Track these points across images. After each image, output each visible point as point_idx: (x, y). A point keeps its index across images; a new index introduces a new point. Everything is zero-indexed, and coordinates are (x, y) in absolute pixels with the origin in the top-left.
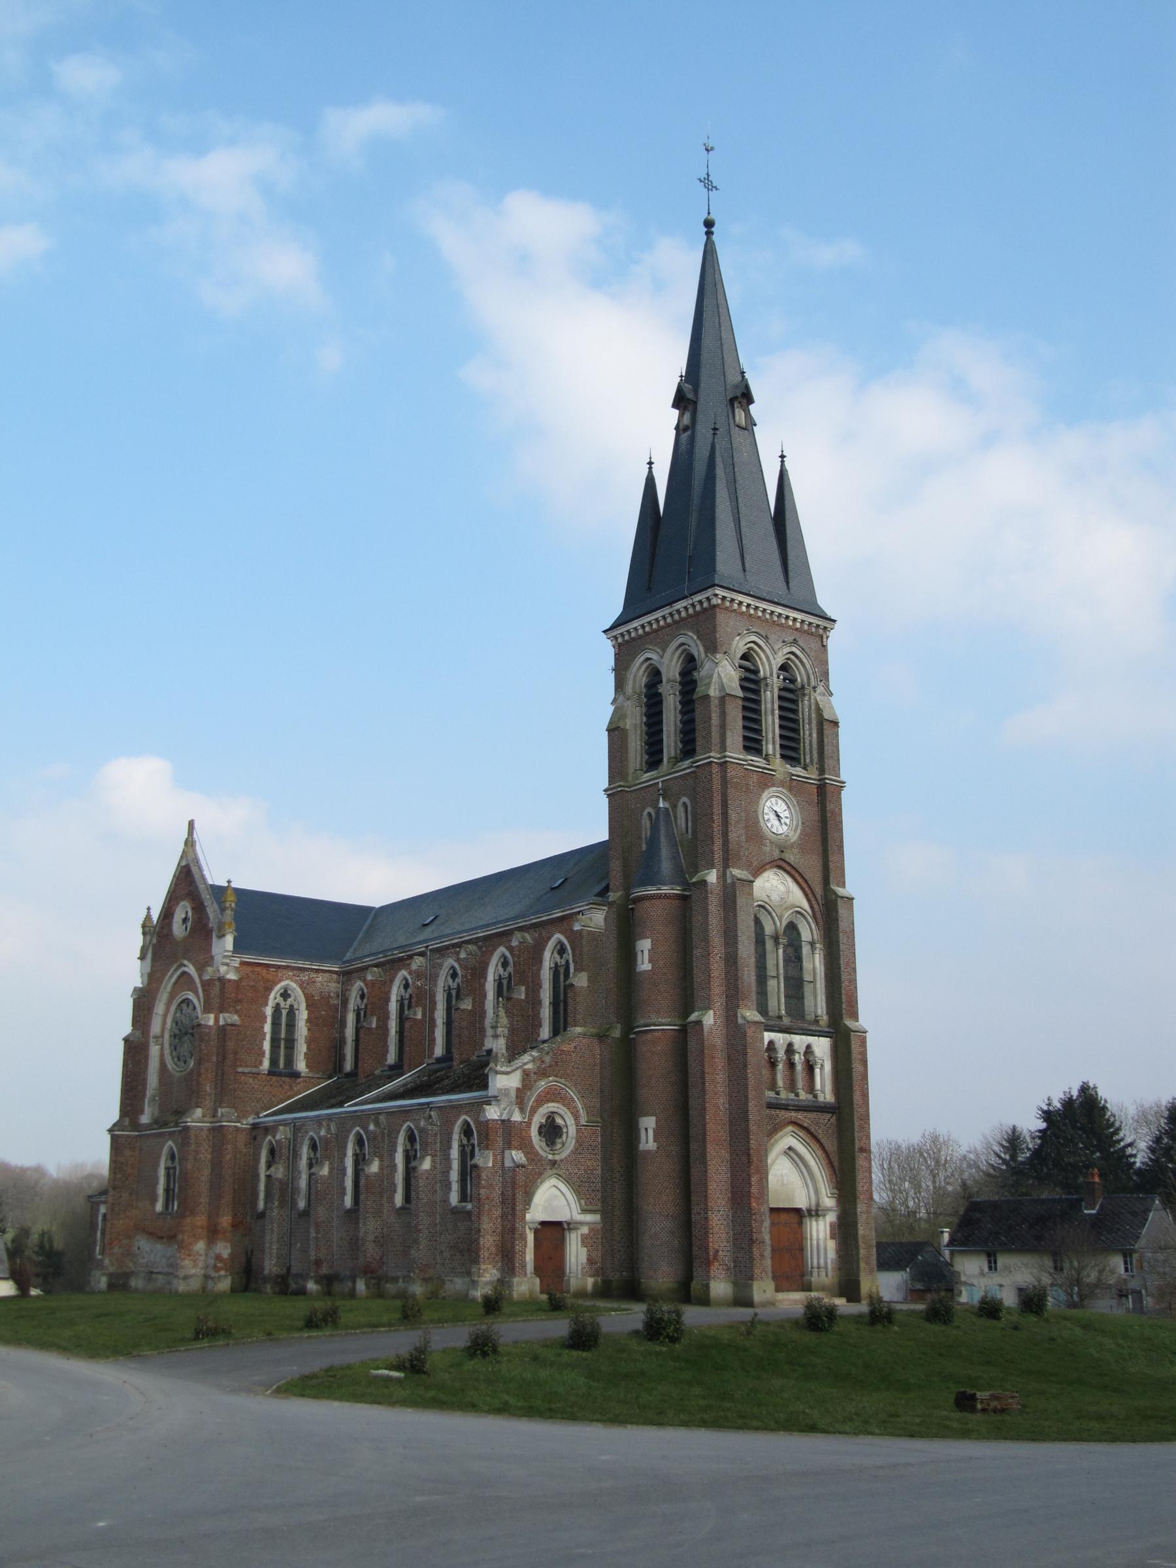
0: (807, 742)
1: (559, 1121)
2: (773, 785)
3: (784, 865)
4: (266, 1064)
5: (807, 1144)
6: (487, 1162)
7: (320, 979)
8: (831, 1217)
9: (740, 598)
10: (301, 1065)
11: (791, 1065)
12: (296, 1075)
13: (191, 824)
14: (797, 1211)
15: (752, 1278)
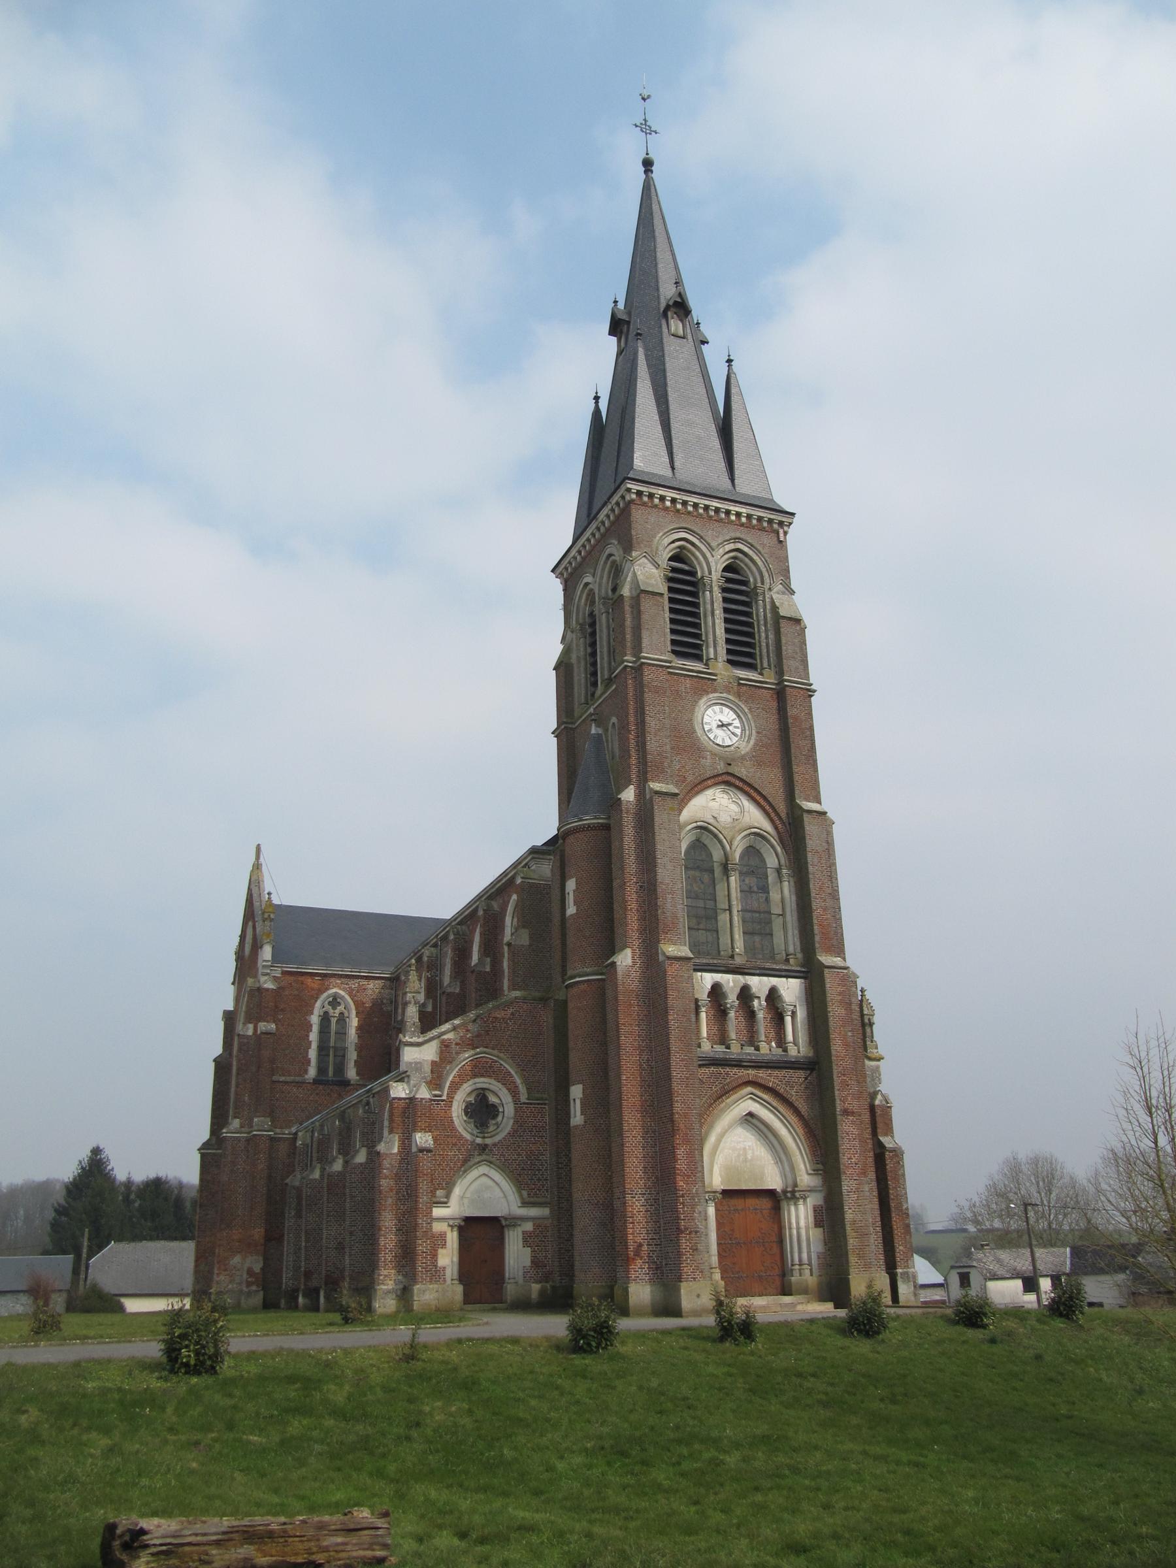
0: (764, 644)
1: (493, 1099)
2: (715, 691)
3: (733, 780)
4: (312, 1072)
5: (774, 1110)
6: (392, 1148)
7: (371, 986)
8: (813, 1200)
9: (661, 492)
10: (351, 1073)
11: (751, 1015)
12: (345, 1083)
13: (258, 848)
14: (771, 1193)
15: (680, 1279)
